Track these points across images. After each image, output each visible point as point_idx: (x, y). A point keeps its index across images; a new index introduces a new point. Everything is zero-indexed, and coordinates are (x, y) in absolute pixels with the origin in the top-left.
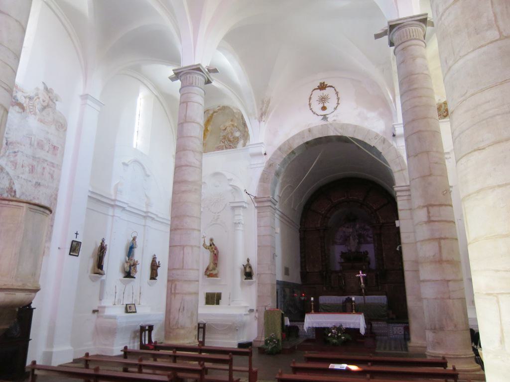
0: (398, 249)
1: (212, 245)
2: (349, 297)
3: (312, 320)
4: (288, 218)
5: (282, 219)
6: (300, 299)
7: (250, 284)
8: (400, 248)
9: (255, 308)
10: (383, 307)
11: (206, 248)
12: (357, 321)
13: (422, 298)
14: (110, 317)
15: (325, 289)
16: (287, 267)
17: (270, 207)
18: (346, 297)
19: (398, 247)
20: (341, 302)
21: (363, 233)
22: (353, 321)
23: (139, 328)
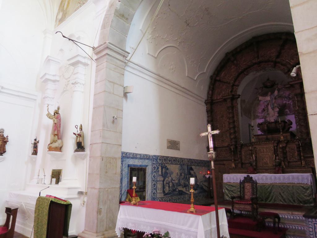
0: (293, 74)
1: (56, 113)
2: (248, 176)
3: (128, 217)
4: (201, 97)
5: (161, 84)
6: (204, 176)
7: (83, 158)
8: (299, 71)
9: (84, 190)
10: (307, 189)
11: (50, 118)
12: (193, 229)
13: (39, 198)
14: (311, 183)
15: (233, 165)
16: (175, 139)
17: (107, 56)
18: (245, 175)
19: (294, 70)
20: (239, 181)
21: (287, 103)
22: (185, 228)
23: (34, 203)
